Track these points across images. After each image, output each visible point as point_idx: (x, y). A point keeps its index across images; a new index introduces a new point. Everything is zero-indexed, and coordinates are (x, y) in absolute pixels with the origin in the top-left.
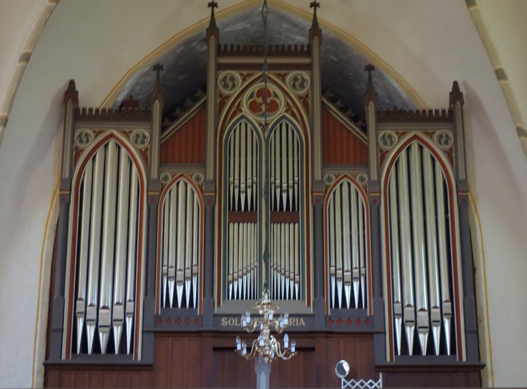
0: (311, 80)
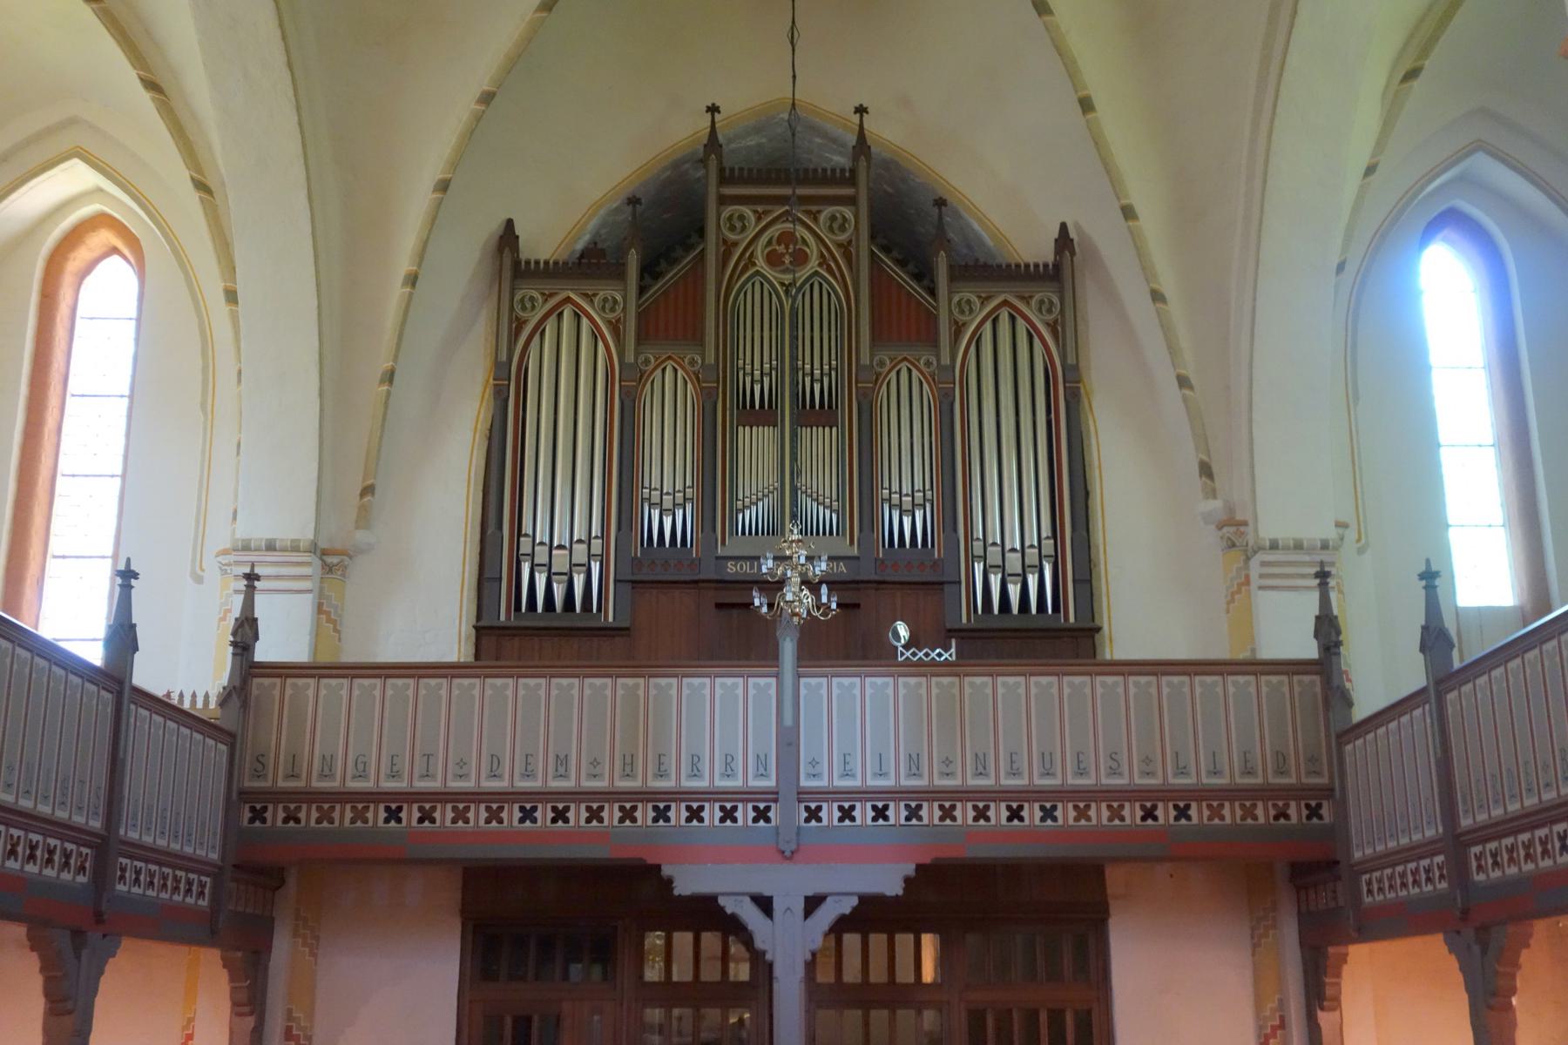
0: (856, 220)
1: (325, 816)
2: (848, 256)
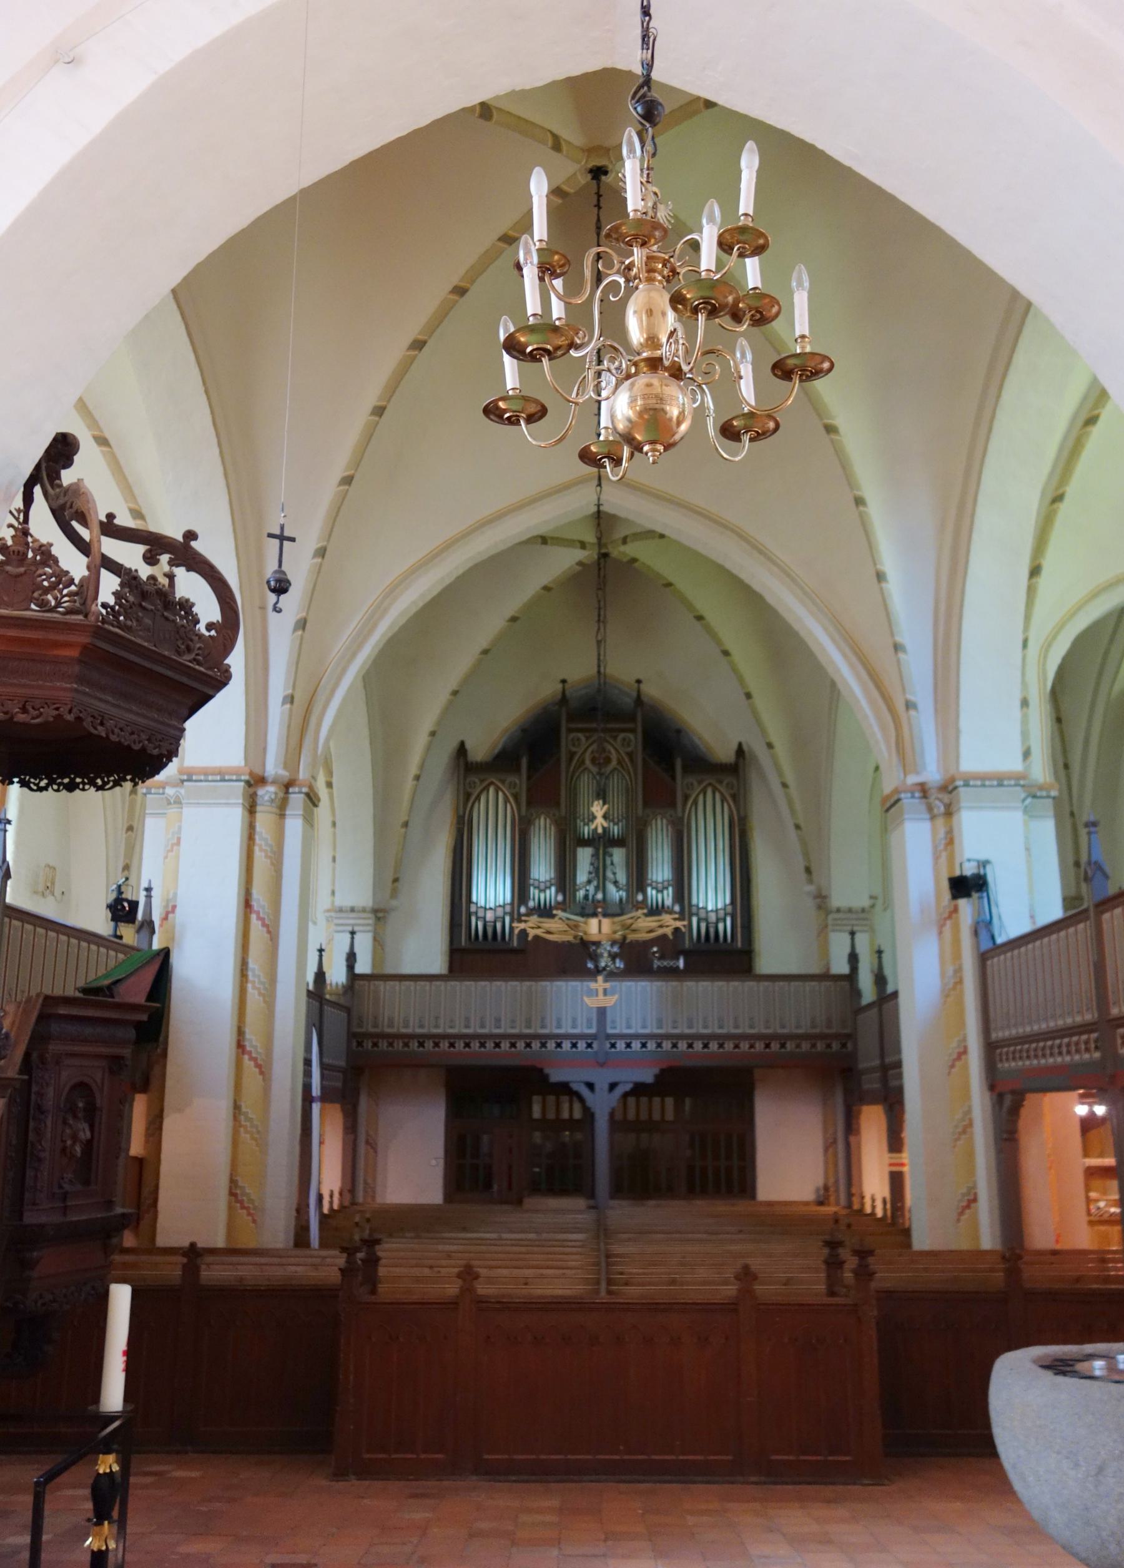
0: (635, 740)
2: (631, 760)
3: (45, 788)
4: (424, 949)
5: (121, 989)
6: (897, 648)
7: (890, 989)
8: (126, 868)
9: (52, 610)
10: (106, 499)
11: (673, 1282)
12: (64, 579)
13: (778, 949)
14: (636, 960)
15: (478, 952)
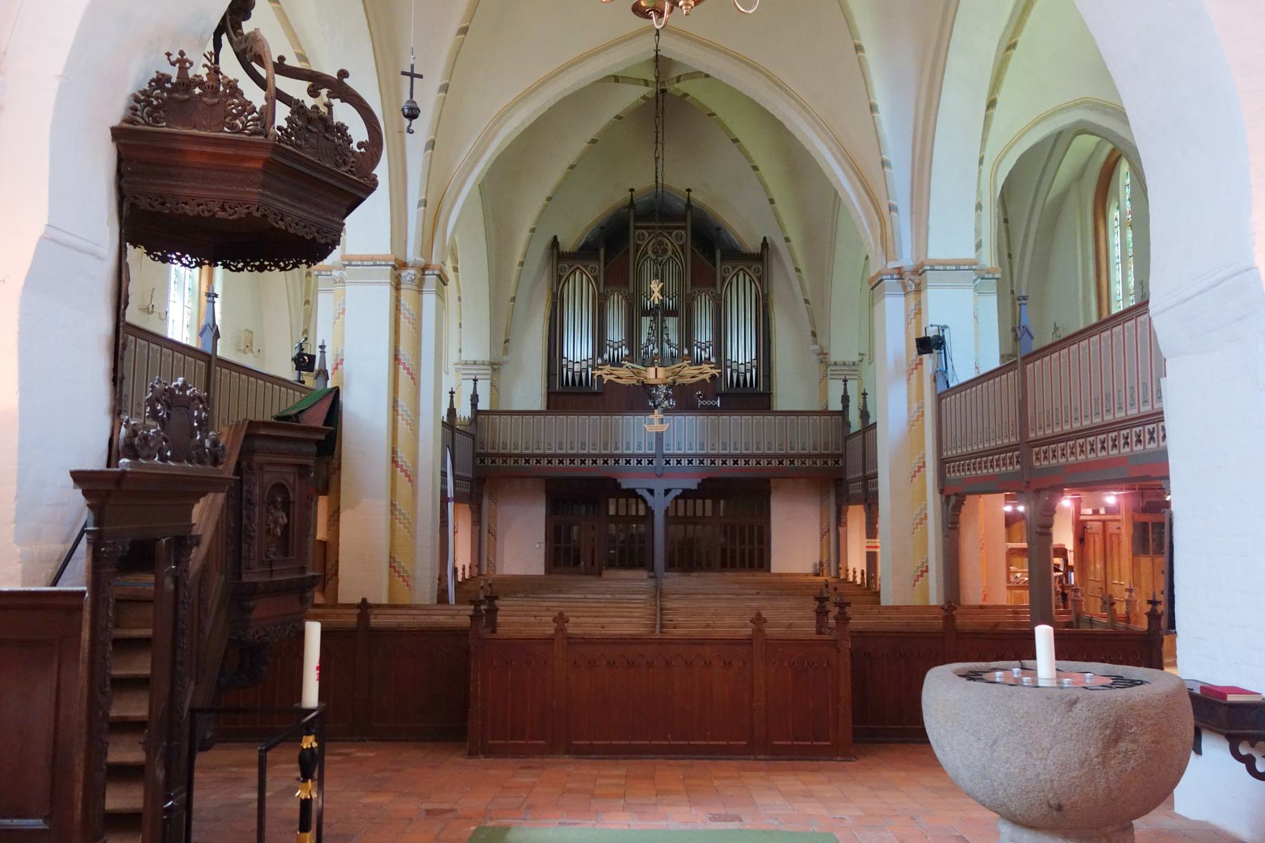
0: (686, 235)
1: (505, 462)
3: (242, 269)
4: (528, 392)
5: (305, 416)
6: (884, 164)
7: (871, 421)
8: (306, 331)
9: (240, 132)
10: (277, 46)
11: (708, 626)
12: (247, 106)
13: (790, 392)
14: (686, 399)
15: (567, 394)
